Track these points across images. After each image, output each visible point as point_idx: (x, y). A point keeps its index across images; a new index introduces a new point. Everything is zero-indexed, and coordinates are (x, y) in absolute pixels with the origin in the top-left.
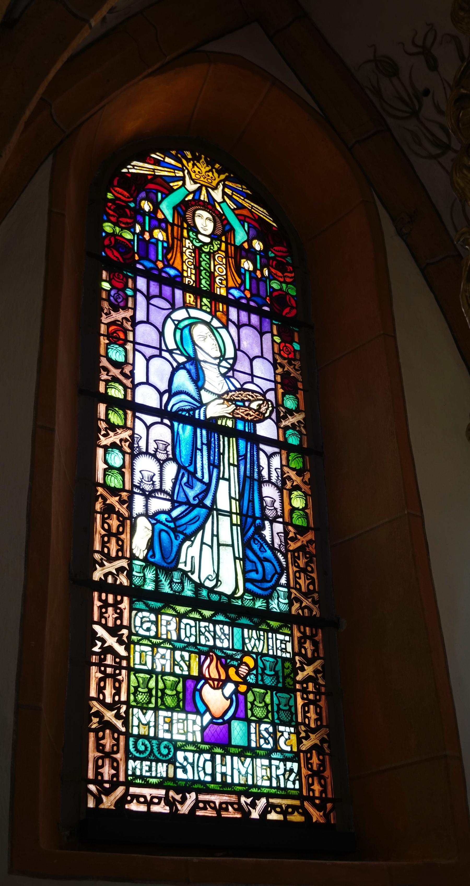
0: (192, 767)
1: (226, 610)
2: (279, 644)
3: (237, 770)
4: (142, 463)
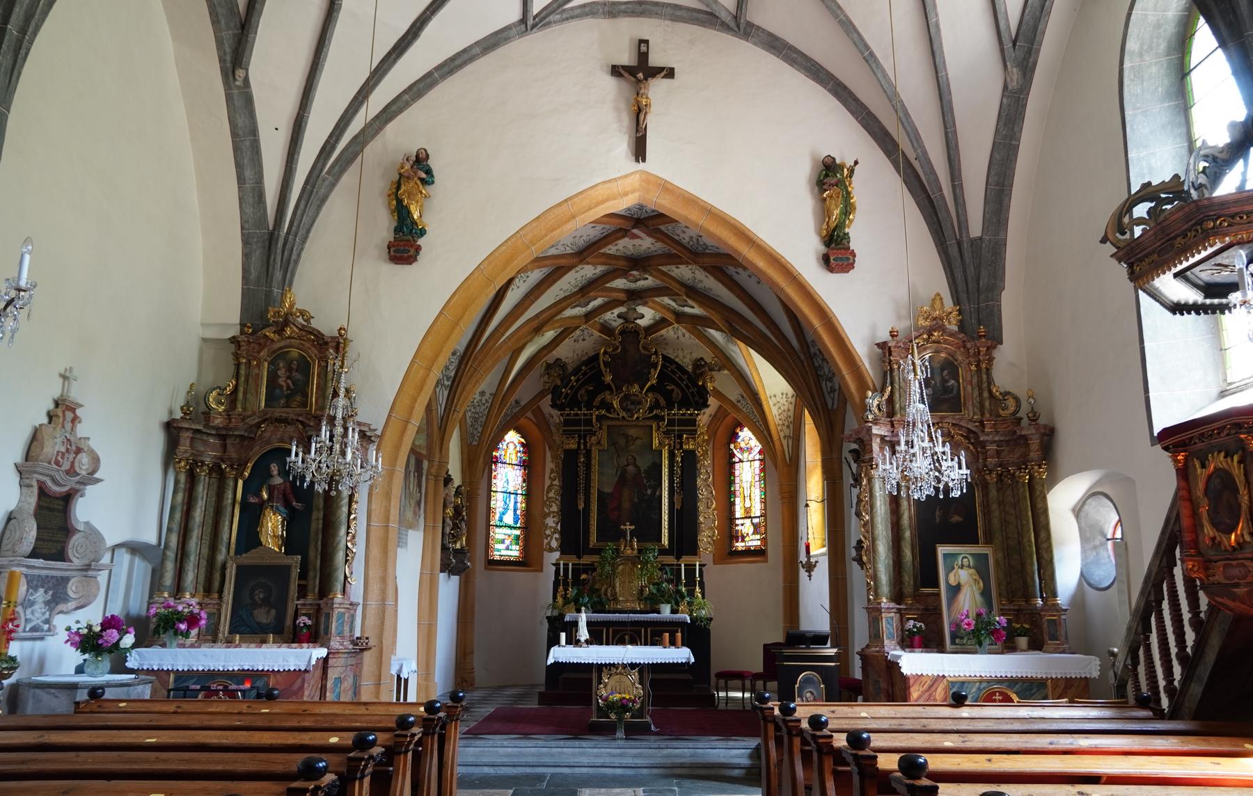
0: (504, 553)
1: (510, 527)
2: (518, 532)
3: (509, 553)
4: (497, 502)
